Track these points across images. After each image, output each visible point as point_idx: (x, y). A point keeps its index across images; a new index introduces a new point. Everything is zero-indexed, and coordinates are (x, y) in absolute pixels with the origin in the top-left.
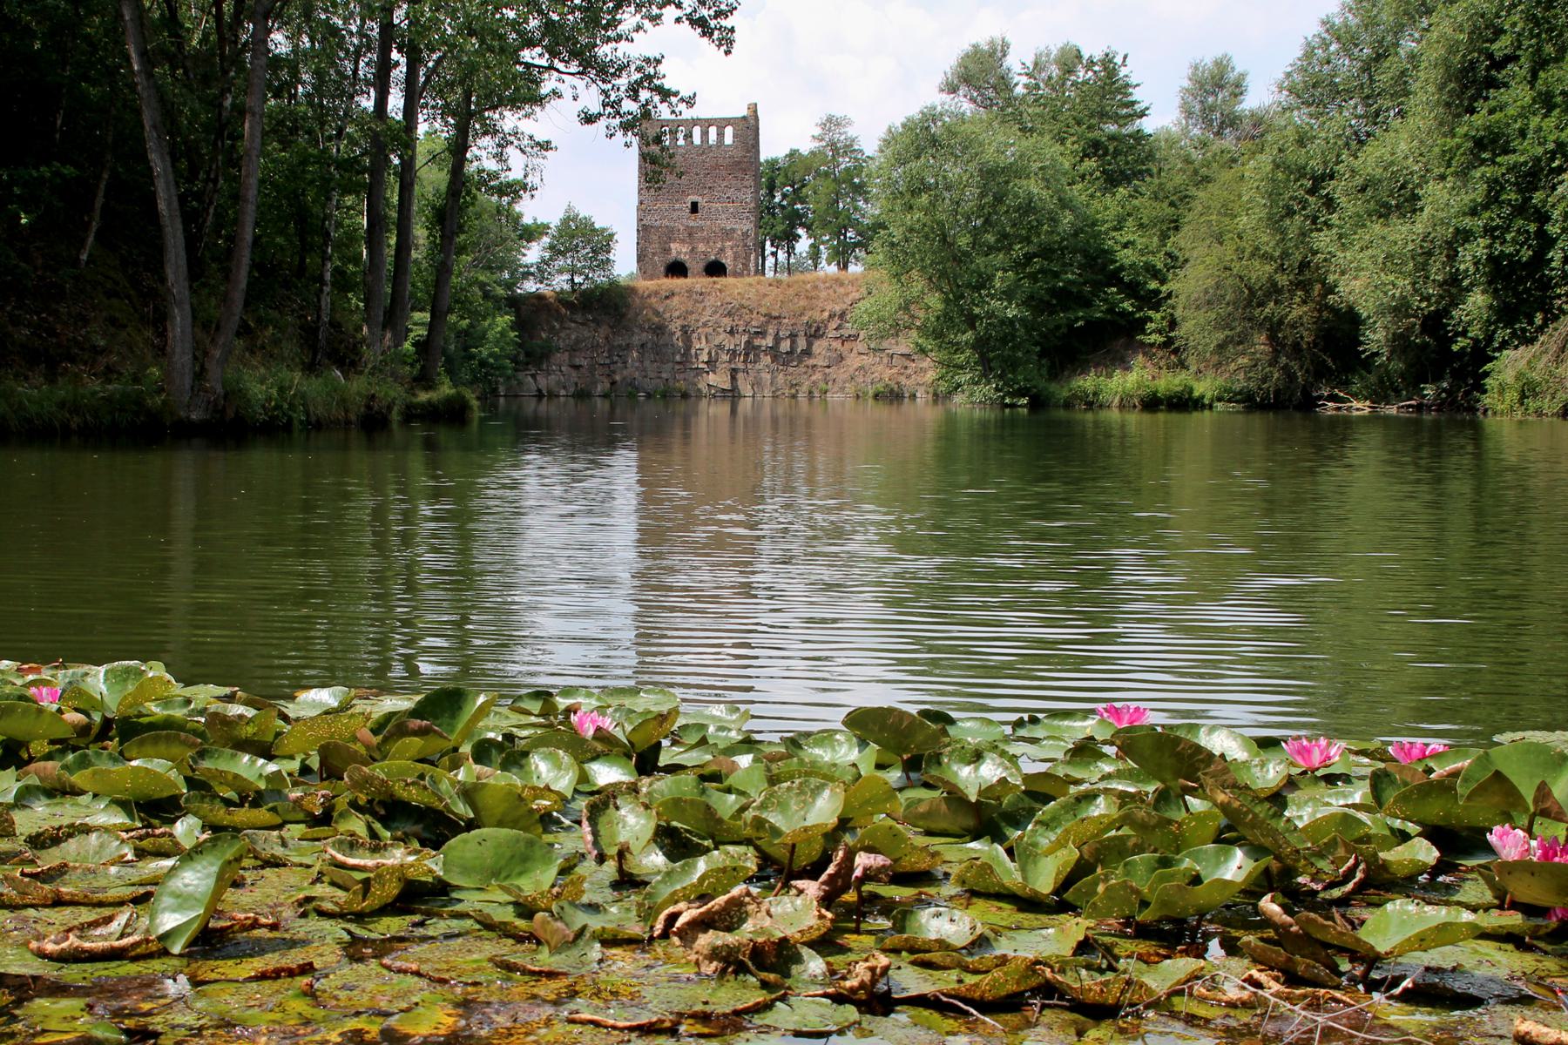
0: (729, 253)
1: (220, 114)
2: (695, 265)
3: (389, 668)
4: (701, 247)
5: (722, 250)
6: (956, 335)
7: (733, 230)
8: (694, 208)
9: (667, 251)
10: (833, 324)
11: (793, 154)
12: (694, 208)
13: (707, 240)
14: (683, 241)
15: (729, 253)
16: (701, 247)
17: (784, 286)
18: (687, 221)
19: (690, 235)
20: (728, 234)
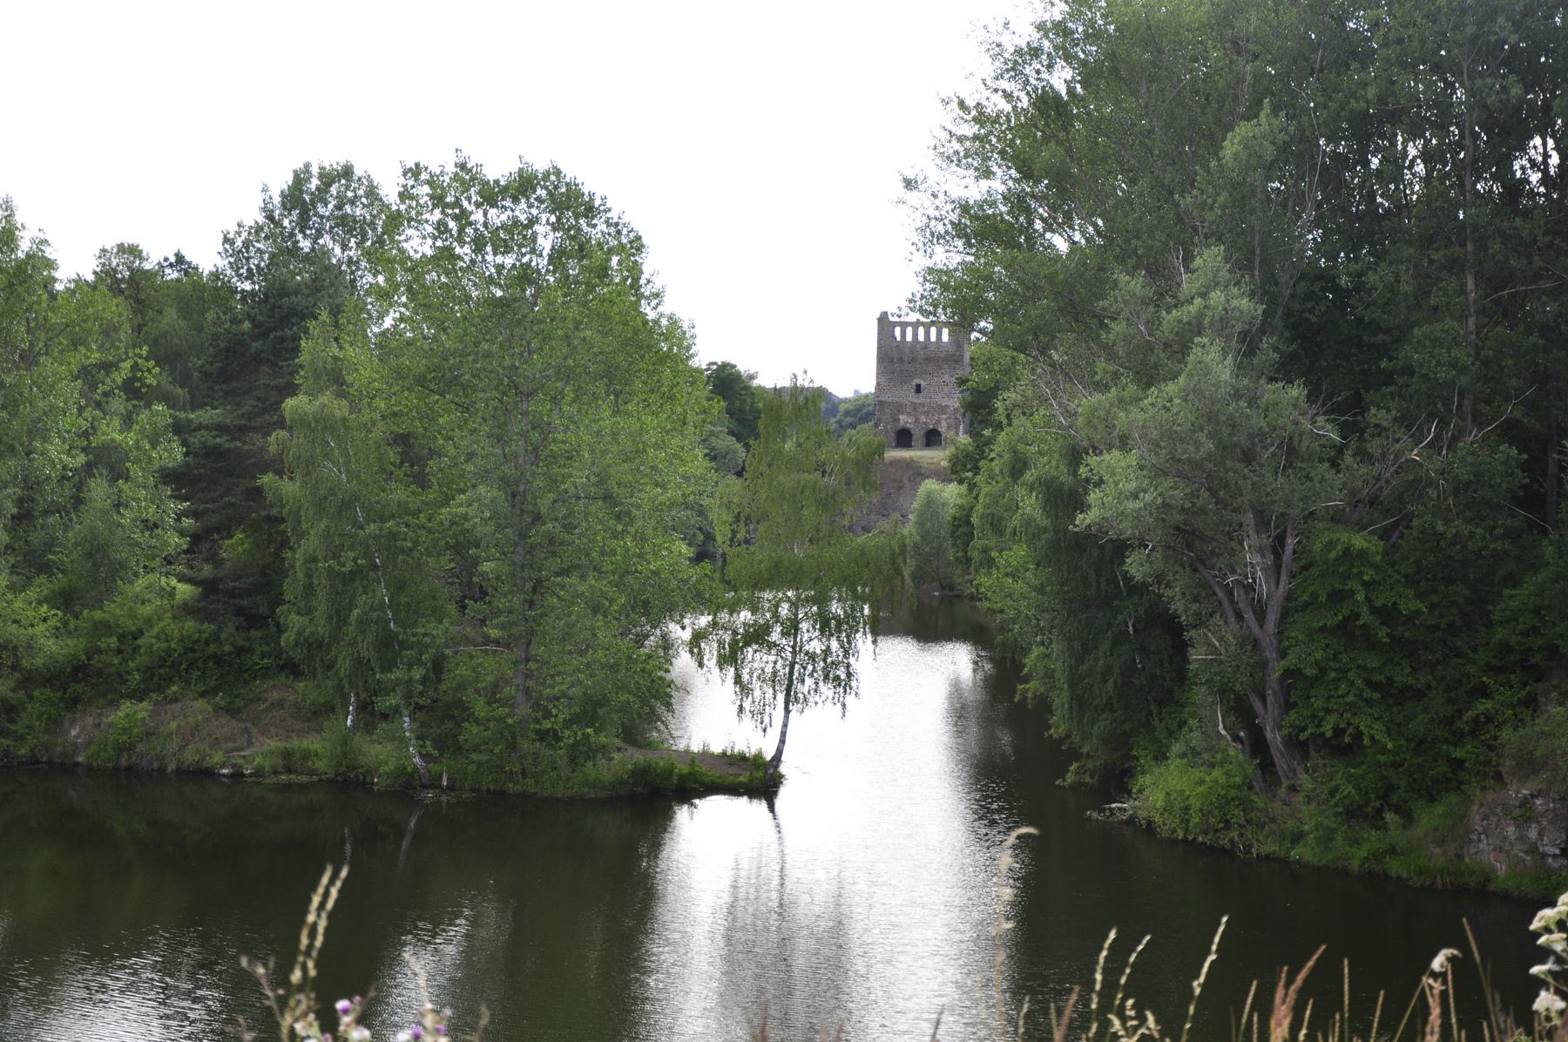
0: (944, 424)
1: (1037, 1011)
2: (918, 435)
3: (601, 707)
4: (923, 419)
5: (939, 421)
6: (1472, 535)
7: (947, 407)
8: (918, 389)
9: (898, 420)
10: (392, 360)
11: (675, 332)
12: (918, 389)
13: (927, 414)
14: (909, 414)
15: (944, 424)
16: (923, 419)
17: (918, 435)
18: (913, 397)
19: (915, 409)
20: (943, 409)
